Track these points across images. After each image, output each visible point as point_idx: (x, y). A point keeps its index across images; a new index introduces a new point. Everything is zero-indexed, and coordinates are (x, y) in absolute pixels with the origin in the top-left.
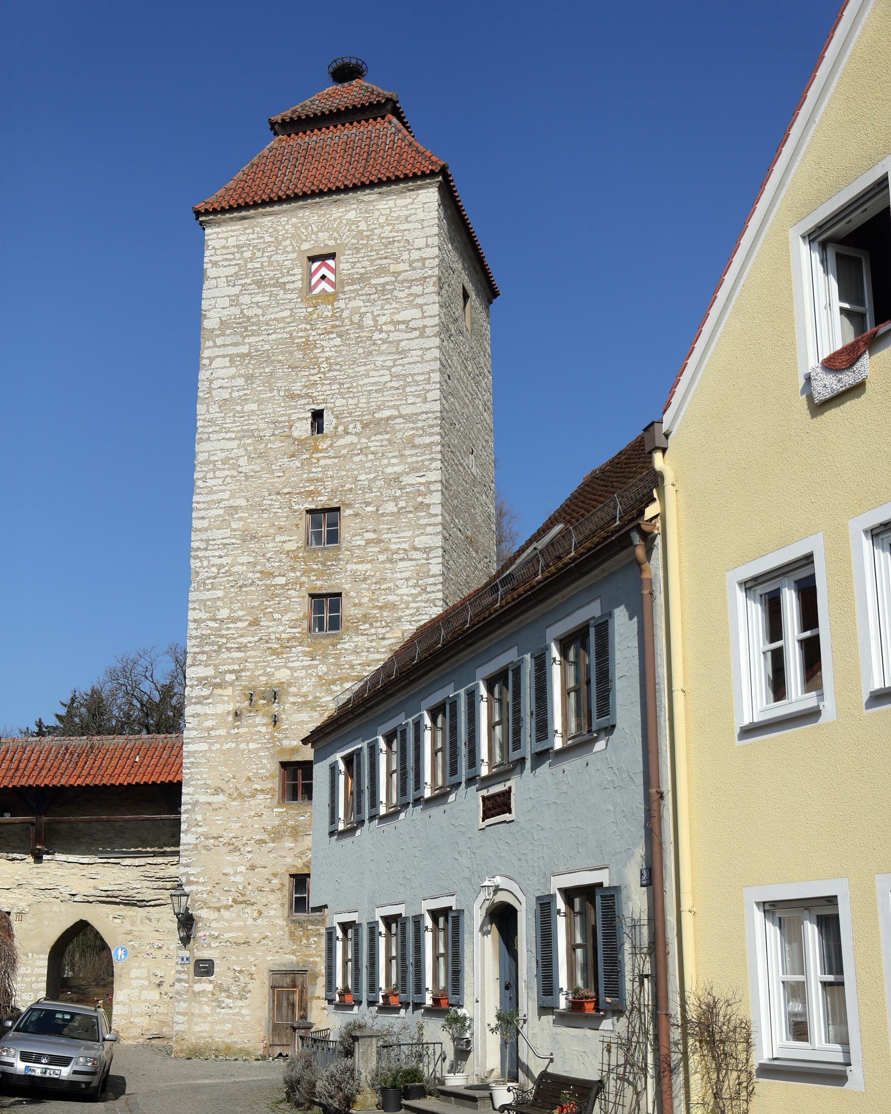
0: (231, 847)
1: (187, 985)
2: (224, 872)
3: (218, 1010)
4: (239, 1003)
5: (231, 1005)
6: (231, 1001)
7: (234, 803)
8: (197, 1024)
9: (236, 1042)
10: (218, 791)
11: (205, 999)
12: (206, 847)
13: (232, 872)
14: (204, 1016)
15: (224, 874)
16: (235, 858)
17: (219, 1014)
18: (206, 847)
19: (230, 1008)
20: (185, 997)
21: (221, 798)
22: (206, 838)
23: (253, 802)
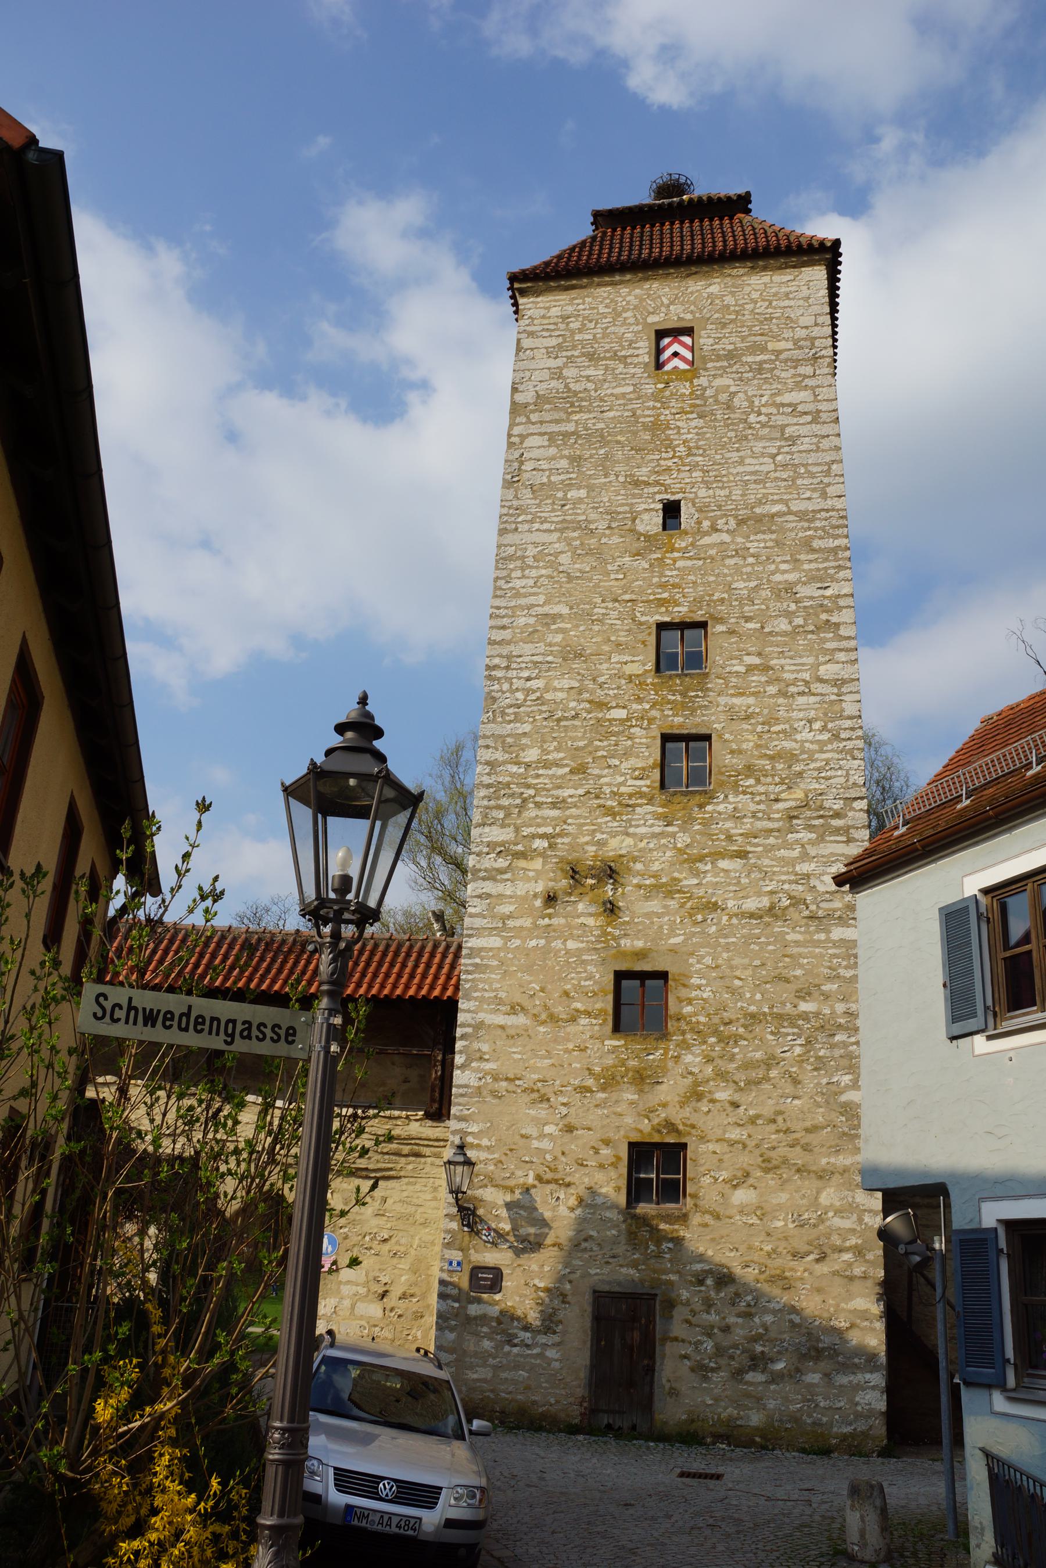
0: (535, 1095)
1: (456, 1305)
2: (523, 1132)
3: (507, 1348)
4: (542, 1339)
5: (529, 1342)
6: (528, 1335)
7: (542, 1029)
8: (471, 1367)
9: (534, 1402)
10: (515, 1009)
11: (485, 1329)
12: (495, 1094)
13: (535, 1134)
14: (484, 1356)
15: (523, 1136)
16: (541, 1112)
17: (509, 1353)
18: (495, 1094)
19: (527, 1346)
20: (453, 1323)
21: (521, 1020)
22: (496, 1079)
23: (571, 1029)
